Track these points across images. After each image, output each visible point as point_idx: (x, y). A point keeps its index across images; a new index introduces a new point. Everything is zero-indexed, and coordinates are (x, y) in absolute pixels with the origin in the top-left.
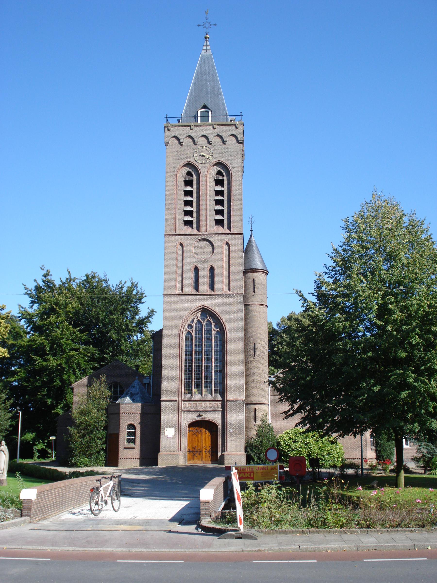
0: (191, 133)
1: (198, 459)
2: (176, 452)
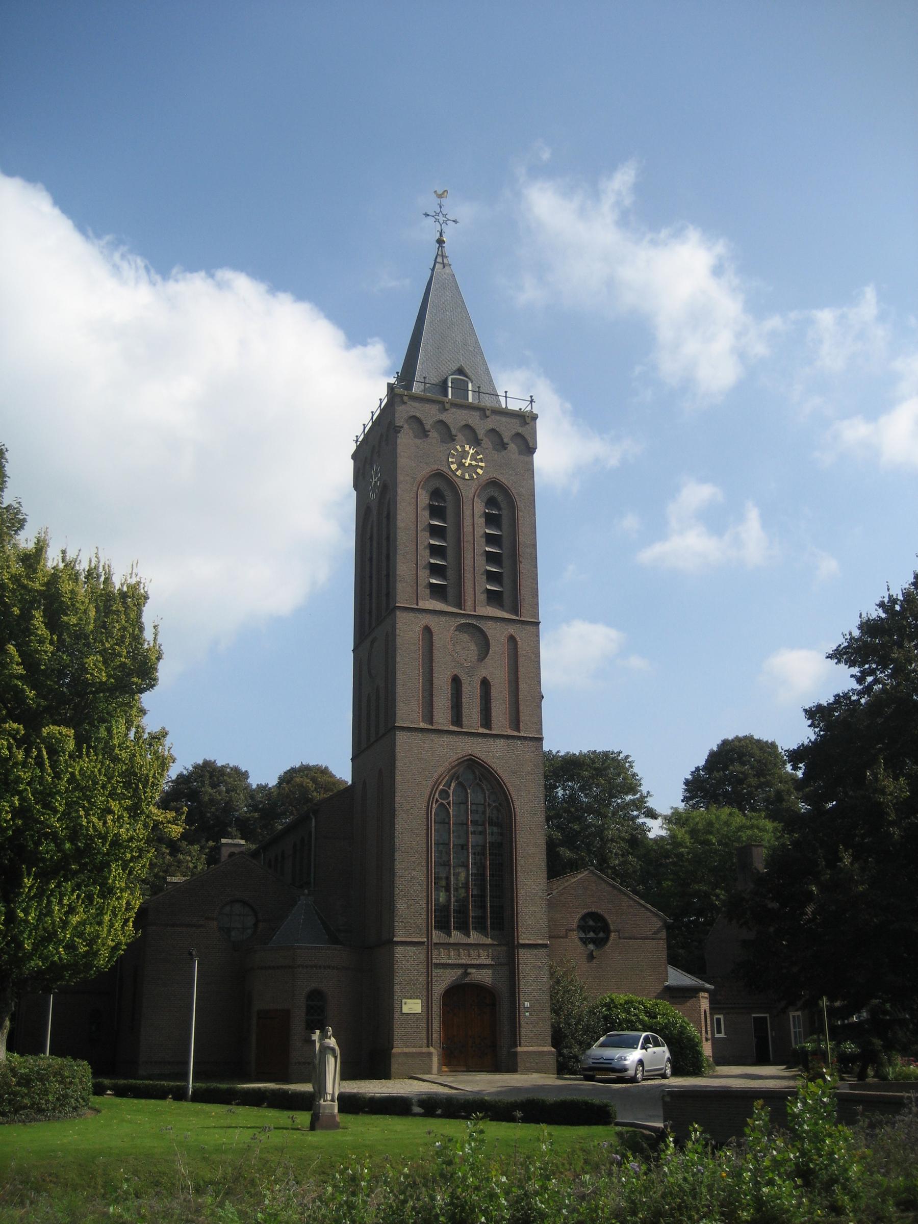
0: (444, 417)
2: (425, 1050)
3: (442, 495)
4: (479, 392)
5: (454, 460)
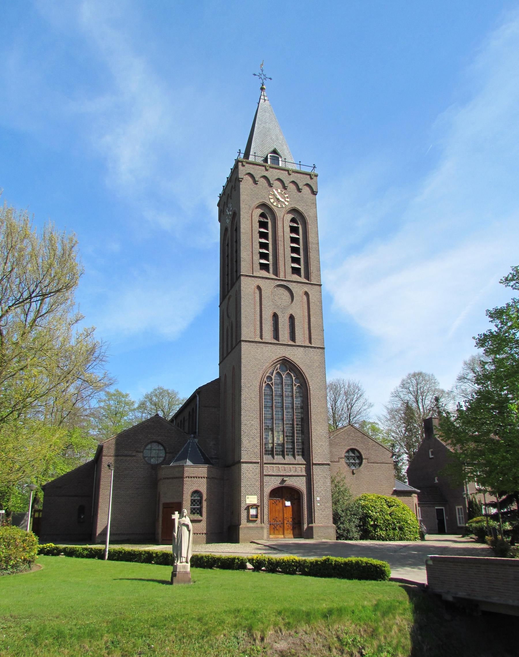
0: (266, 174)
1: (279, 532)
3: (267, 213)
4: (285, 162)
5: (272, 197)
